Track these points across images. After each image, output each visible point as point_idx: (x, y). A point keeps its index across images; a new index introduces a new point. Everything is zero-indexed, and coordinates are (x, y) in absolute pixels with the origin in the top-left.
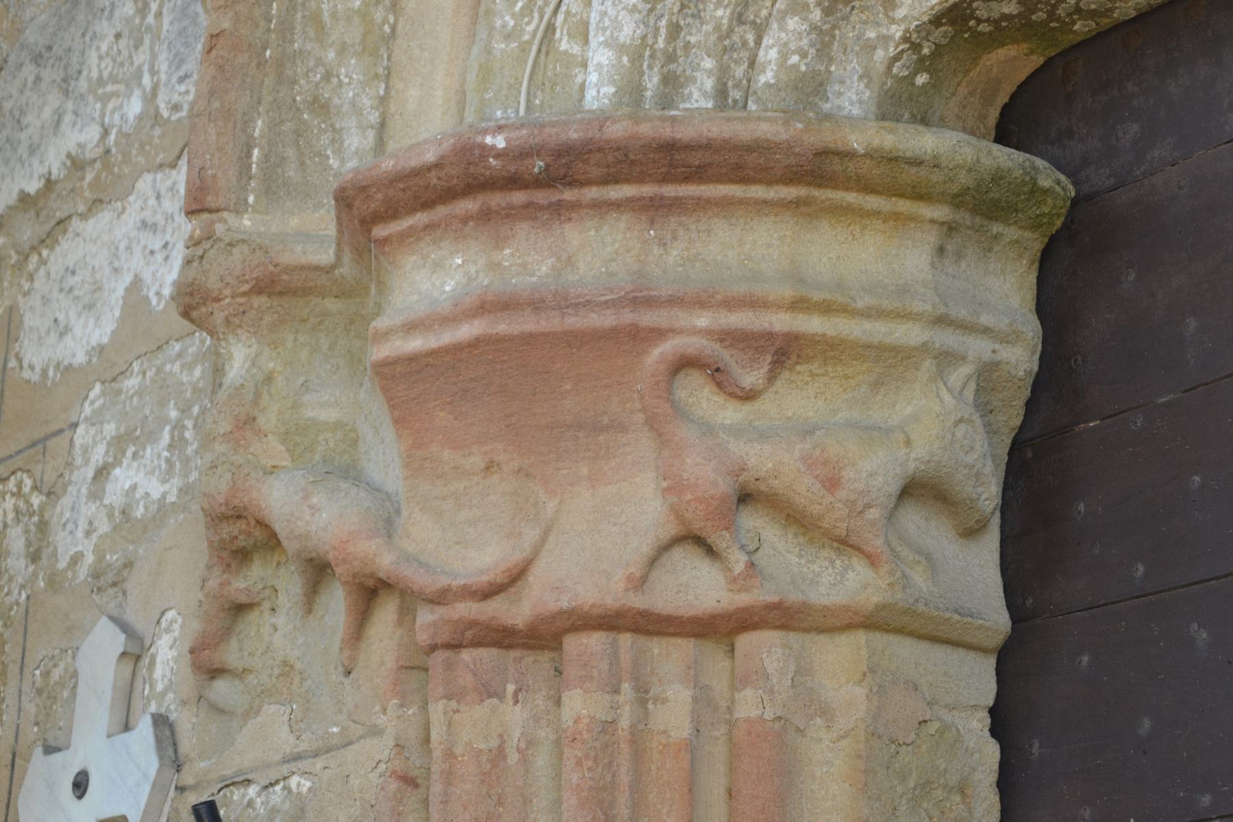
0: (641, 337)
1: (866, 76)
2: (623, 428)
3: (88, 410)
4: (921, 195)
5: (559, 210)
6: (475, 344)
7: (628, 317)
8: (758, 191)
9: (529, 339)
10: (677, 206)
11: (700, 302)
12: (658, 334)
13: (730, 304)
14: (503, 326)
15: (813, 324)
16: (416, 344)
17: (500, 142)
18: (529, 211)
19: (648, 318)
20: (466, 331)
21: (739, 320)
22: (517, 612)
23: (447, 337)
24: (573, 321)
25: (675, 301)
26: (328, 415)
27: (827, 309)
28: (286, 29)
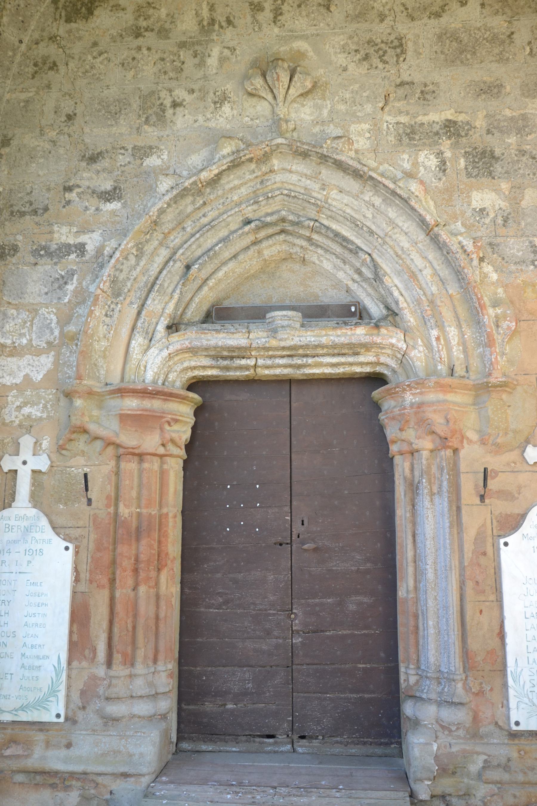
0: (162, 417)
1: (181, 381)
2: (156, 428)
3: (12, 394)
4: (192, 402)
5: (153, 398)
6: (140, 415)
7: (162, 415)
8: (177, 400)
9: (148, 415)
10: (168, 400)
11: (170, 414)
12: (165, 417)
13: (173, 415)
14: (145, 413)
15: (181, 418)
16: (129, 412)
17: (150, 388)
18: (149, 397)
19: (164, 415)
20: (139, 413)
21: (174, 417)
22: (136, 451)
23: (135, 413)
24: (154, 414)
25: (168, 413)
26: (95, 414)
27: (182, 416)
28: (91, 351)
